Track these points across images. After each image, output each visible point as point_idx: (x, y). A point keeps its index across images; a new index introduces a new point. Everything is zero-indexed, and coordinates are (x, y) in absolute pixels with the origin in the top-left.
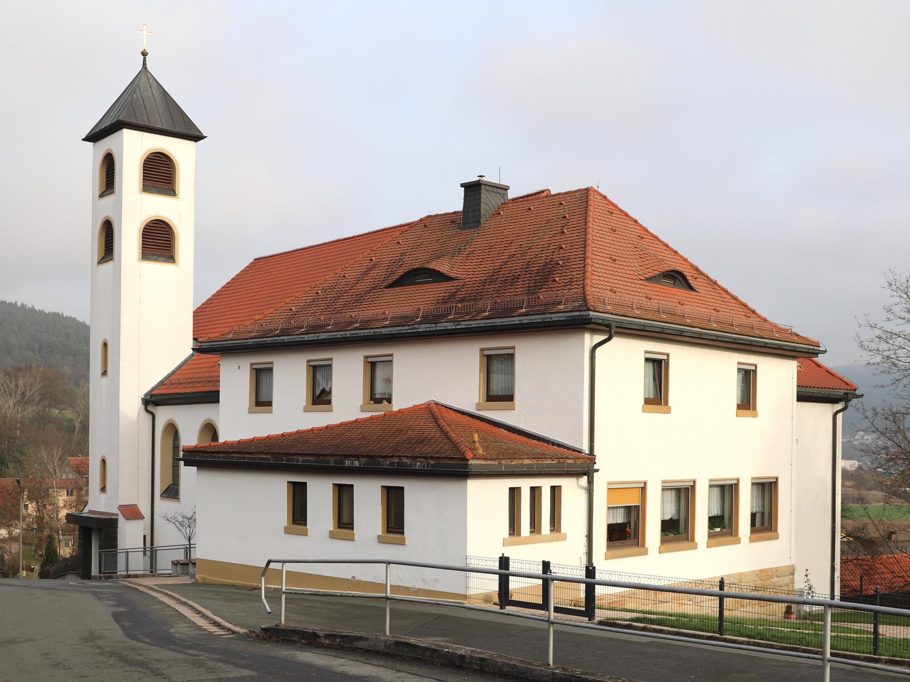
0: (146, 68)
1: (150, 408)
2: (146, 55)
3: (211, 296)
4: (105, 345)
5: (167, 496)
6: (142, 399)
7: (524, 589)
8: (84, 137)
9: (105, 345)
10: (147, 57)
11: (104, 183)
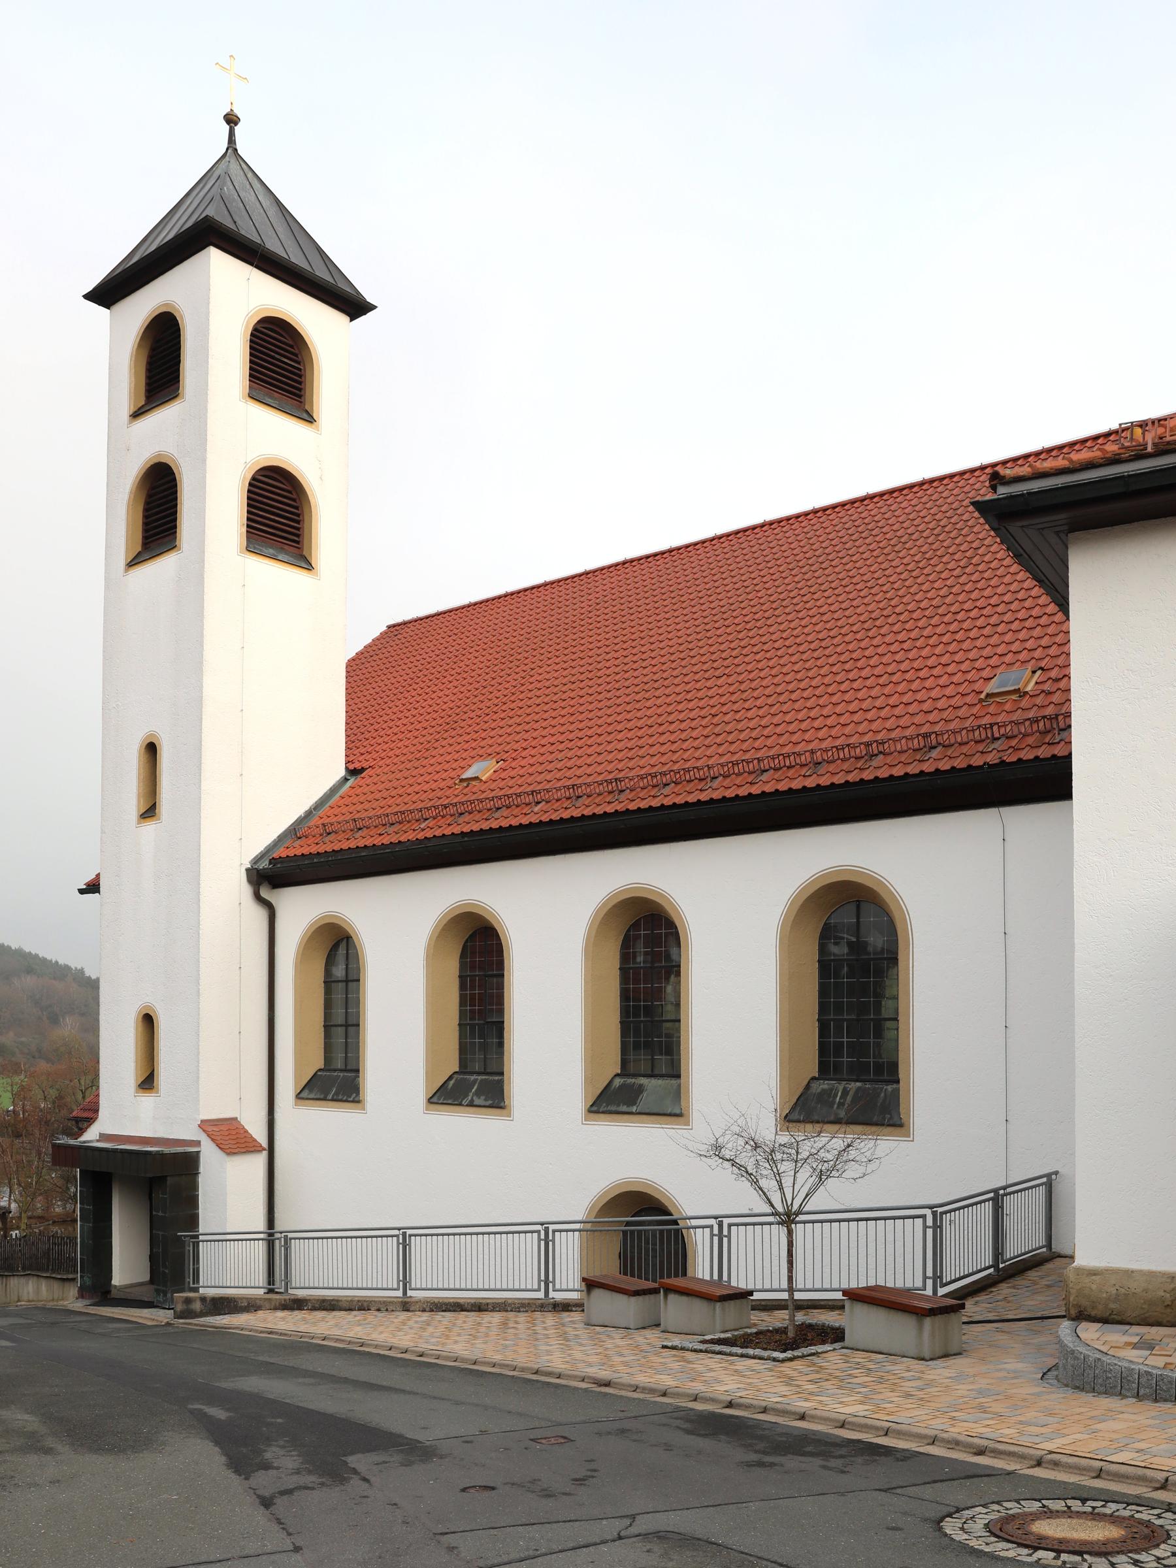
0: (236, 150)
1: (265, 893)
2: (236, 124)
3: (371, 641)
4: (152, 749)
5: (322, 1097)
6: (247, 870)
7: (669, 1269)
8: (89, 288)
9: (152, 749)
10: (238, 129)
11: (143, 388)
